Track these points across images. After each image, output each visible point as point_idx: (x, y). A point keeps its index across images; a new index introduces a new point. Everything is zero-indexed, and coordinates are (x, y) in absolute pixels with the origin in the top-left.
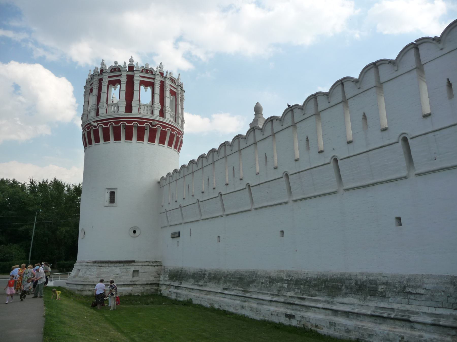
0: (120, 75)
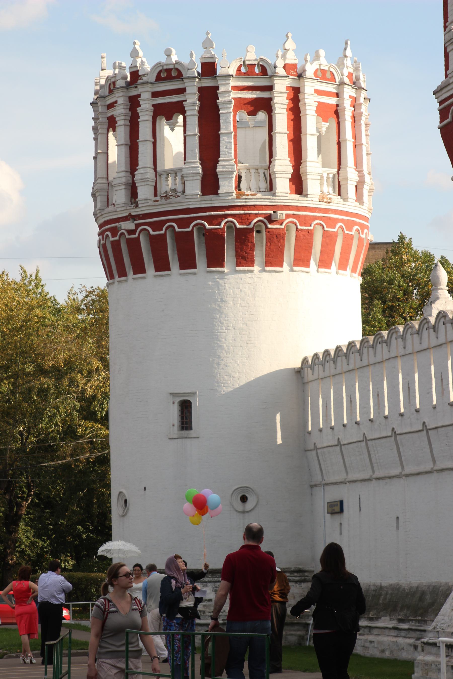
0: (182, 91)
